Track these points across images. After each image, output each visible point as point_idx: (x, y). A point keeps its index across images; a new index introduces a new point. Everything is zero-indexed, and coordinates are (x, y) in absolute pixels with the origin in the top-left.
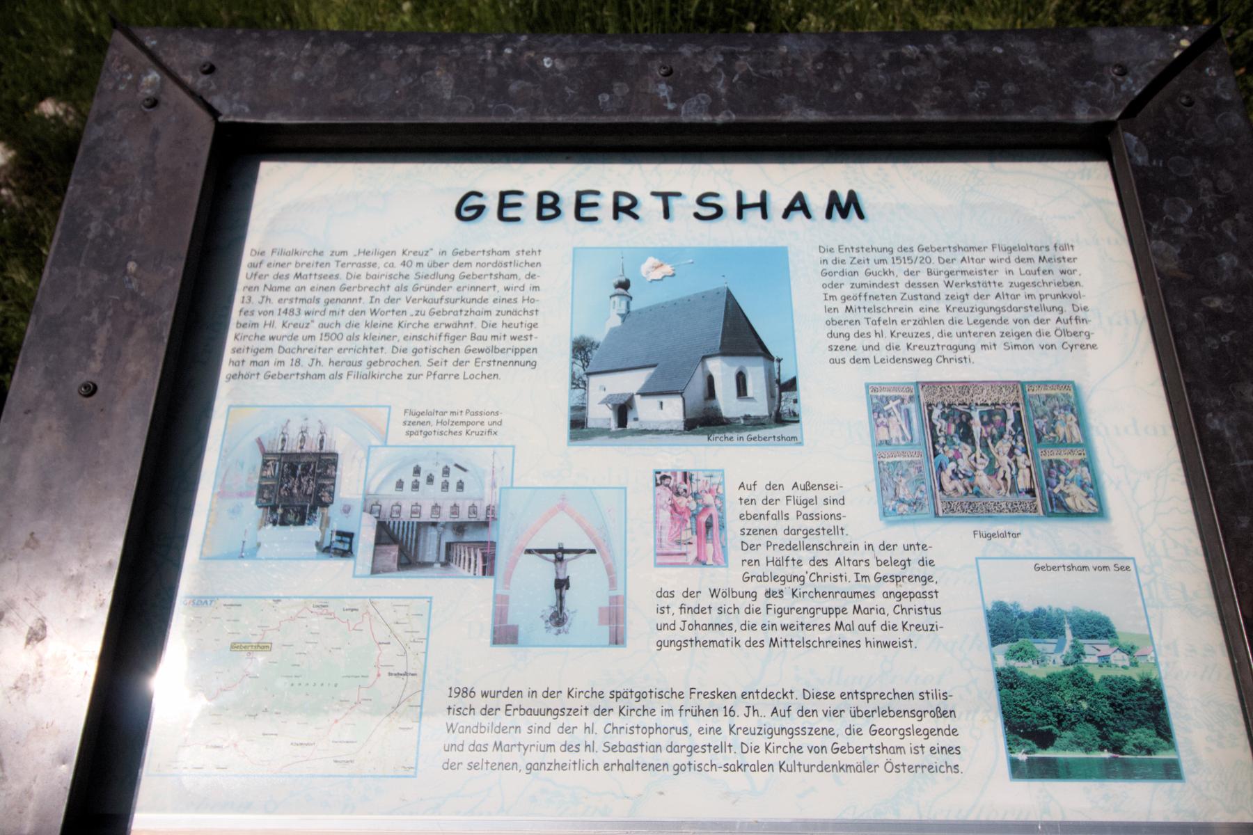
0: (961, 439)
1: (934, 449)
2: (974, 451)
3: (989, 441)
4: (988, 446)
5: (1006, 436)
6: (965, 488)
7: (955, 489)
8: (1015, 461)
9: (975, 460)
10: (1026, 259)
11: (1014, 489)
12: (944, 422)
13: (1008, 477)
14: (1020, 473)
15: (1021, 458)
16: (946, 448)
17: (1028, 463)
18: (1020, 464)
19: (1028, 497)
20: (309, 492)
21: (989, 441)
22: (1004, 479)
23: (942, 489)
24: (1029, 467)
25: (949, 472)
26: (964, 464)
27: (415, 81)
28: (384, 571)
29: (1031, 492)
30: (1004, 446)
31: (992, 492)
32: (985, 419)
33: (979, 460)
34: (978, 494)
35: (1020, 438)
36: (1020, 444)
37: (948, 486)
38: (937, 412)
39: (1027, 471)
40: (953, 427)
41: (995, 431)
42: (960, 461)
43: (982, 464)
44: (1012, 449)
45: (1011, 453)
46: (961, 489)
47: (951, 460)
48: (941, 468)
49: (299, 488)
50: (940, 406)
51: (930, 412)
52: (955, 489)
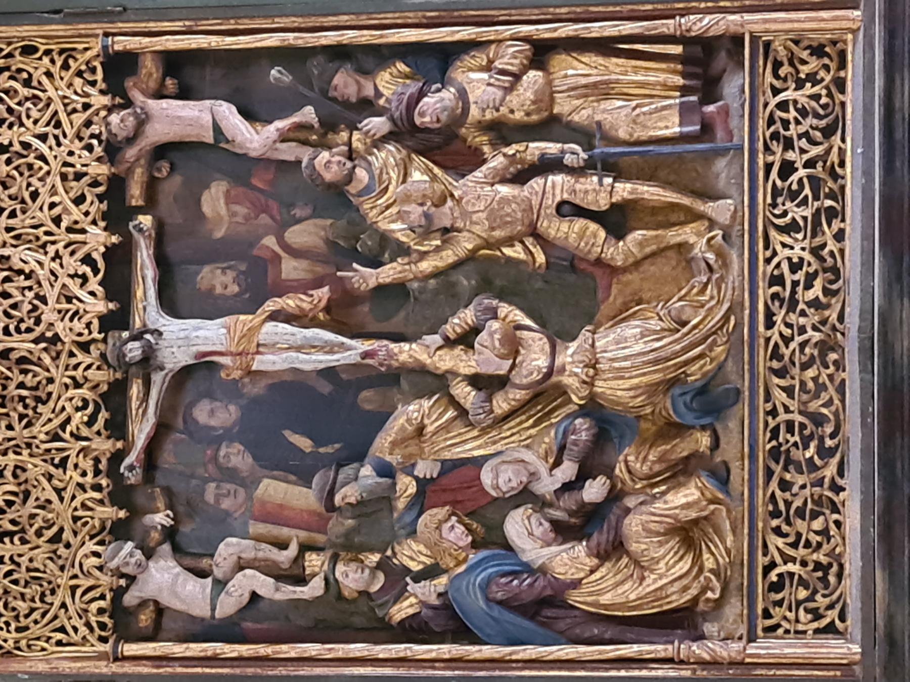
0: (357, 454)
1: (414, 630)
2: (435, 383)
3: (366, 278)
4: (395, 292)
5: (327, 163)
6: (678, 472)
7: (688, 534)
8: (502, 132)
9: (487, 384)
10: (530, 506)
11: (679, 164)
12: (228, 549)
13: (598, 191)
14: (582, 113)
15: (477, 86)
16: (412, 555)
17: (510, 56)
18: (521, 103)
19: (734, 86)
20: (644, 105)
21: (366, 278)
22: (617, 220)
23: (680, 621)
24: (541, 53)
25: (569, 560)
26: (515, 459)
27: (247, 218)
28: (244, 607)
29: (704, 64)
30: (396, 189)
31: (705, 308)
32: (219, 279)
33: (485, 358)
34: (711, 401)
35: (345, 83)
36: (389, 83)
37: (665, 576)
38: (164, 580)
39: (573, 70)
40: (274, 490)
41: (306, 234)
42: (497, 479)
43: (513, 342)
44: (407, 133)
45: (447, 147)
46: (684, 498)
47: (490, 538)
48: (545, 609)
49: (568, 294)
50: (127, 553)
51: (161, 621)
52: (688, 534)
